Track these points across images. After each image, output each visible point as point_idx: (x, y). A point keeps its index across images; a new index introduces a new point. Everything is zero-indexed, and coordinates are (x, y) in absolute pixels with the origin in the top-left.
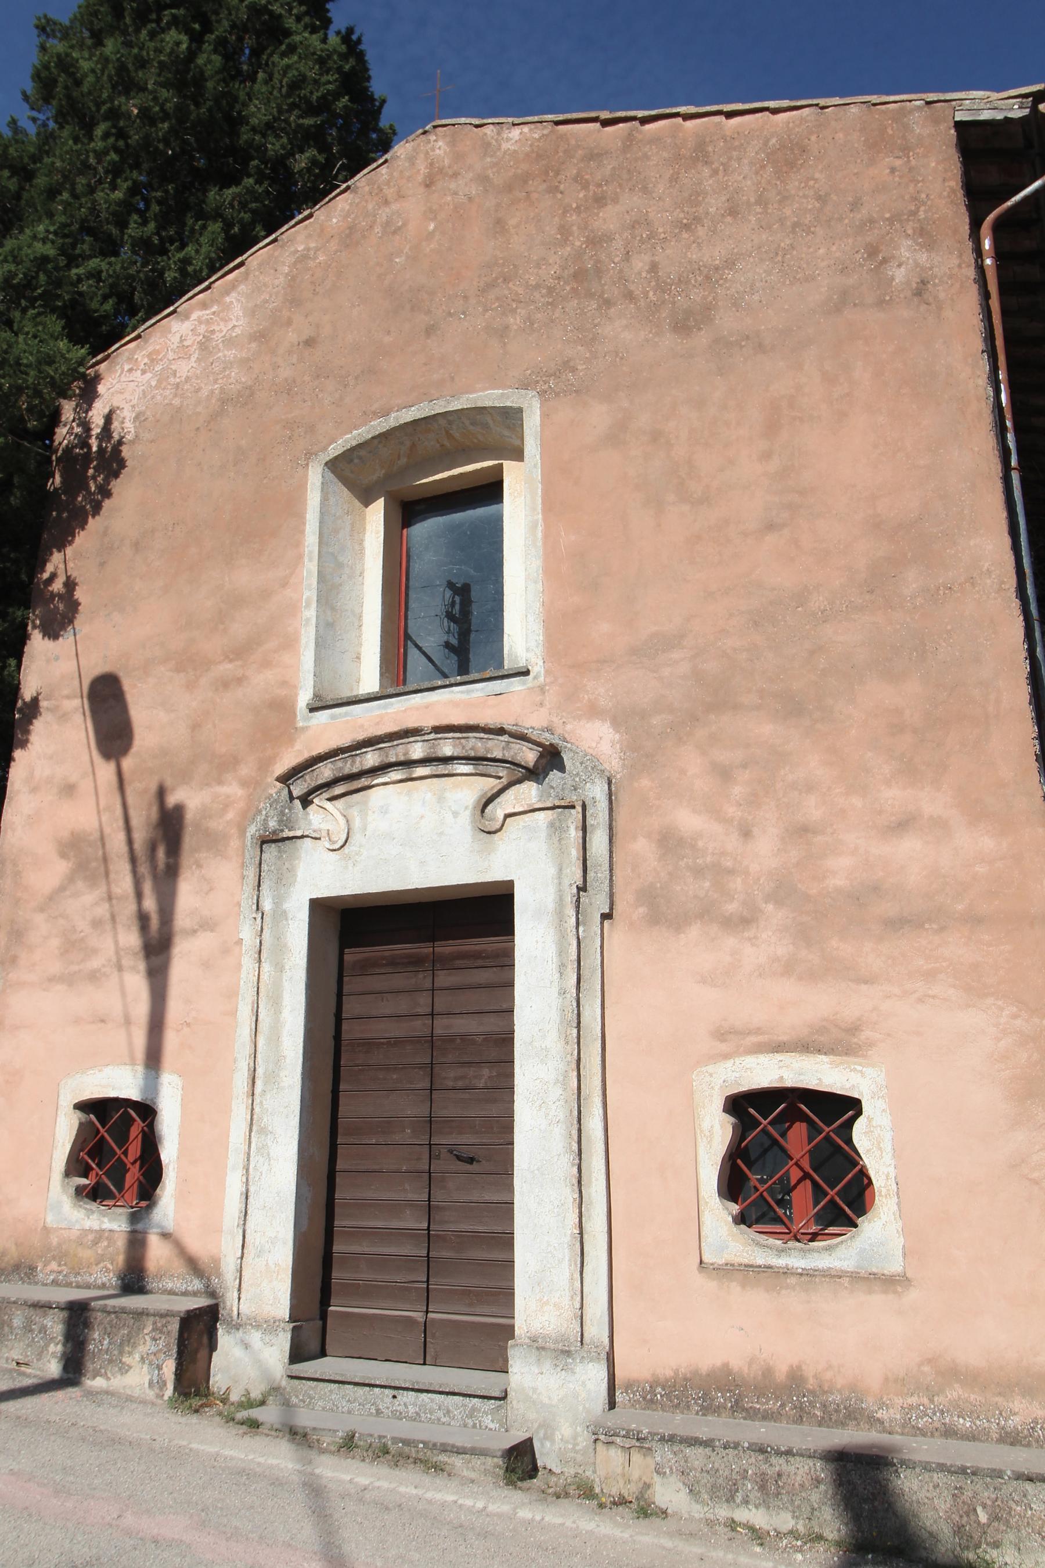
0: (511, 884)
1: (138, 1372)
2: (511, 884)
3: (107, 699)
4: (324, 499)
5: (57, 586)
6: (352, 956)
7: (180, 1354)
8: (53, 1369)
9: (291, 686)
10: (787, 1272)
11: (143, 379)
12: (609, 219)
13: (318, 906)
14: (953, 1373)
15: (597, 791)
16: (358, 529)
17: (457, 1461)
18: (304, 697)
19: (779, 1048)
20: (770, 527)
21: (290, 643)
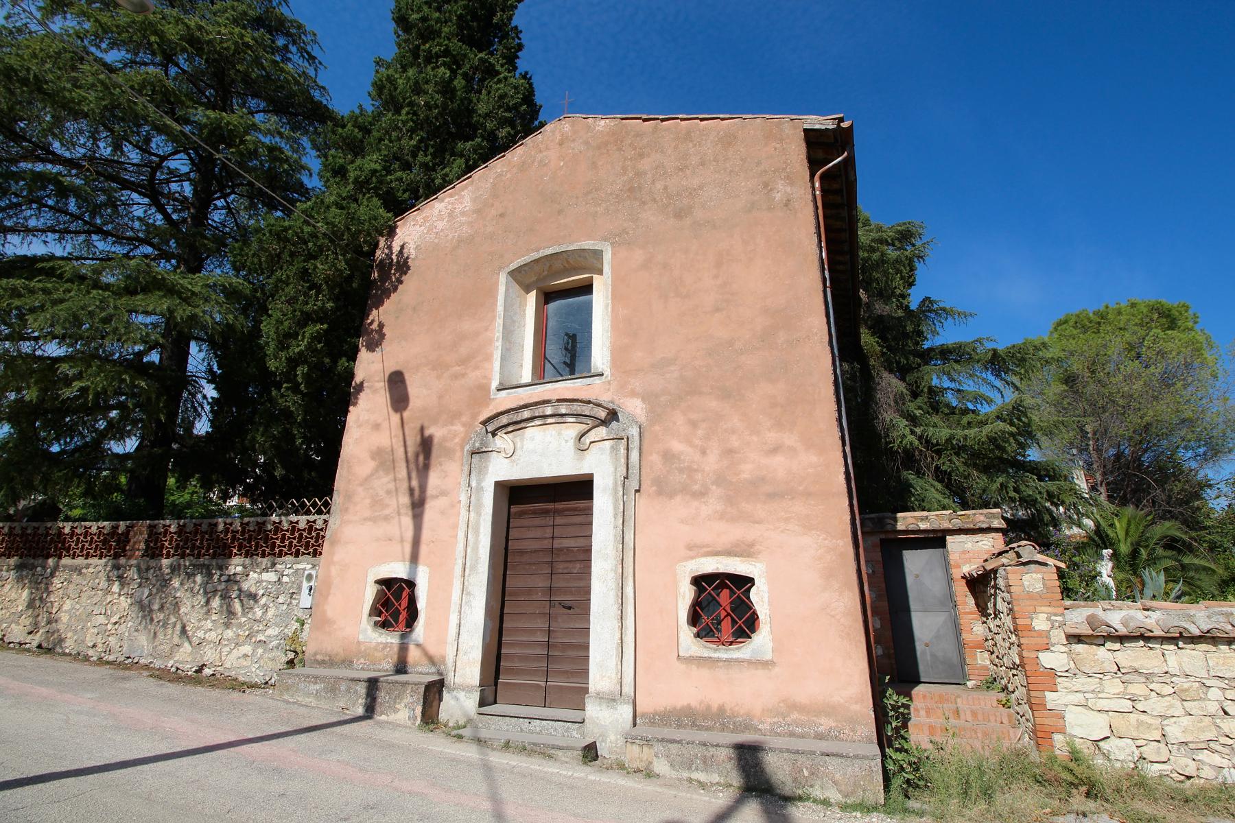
3: (397, 382)
5: (375, 326)
6: (514, 509)
7: (424, 703)
8: (360, 711)
12: (645, 164)
13: (499, 485)
14: (794, 707)
16: (523, 305)
18: (495, 384)
20: (718, 310)
21: (489, 358)
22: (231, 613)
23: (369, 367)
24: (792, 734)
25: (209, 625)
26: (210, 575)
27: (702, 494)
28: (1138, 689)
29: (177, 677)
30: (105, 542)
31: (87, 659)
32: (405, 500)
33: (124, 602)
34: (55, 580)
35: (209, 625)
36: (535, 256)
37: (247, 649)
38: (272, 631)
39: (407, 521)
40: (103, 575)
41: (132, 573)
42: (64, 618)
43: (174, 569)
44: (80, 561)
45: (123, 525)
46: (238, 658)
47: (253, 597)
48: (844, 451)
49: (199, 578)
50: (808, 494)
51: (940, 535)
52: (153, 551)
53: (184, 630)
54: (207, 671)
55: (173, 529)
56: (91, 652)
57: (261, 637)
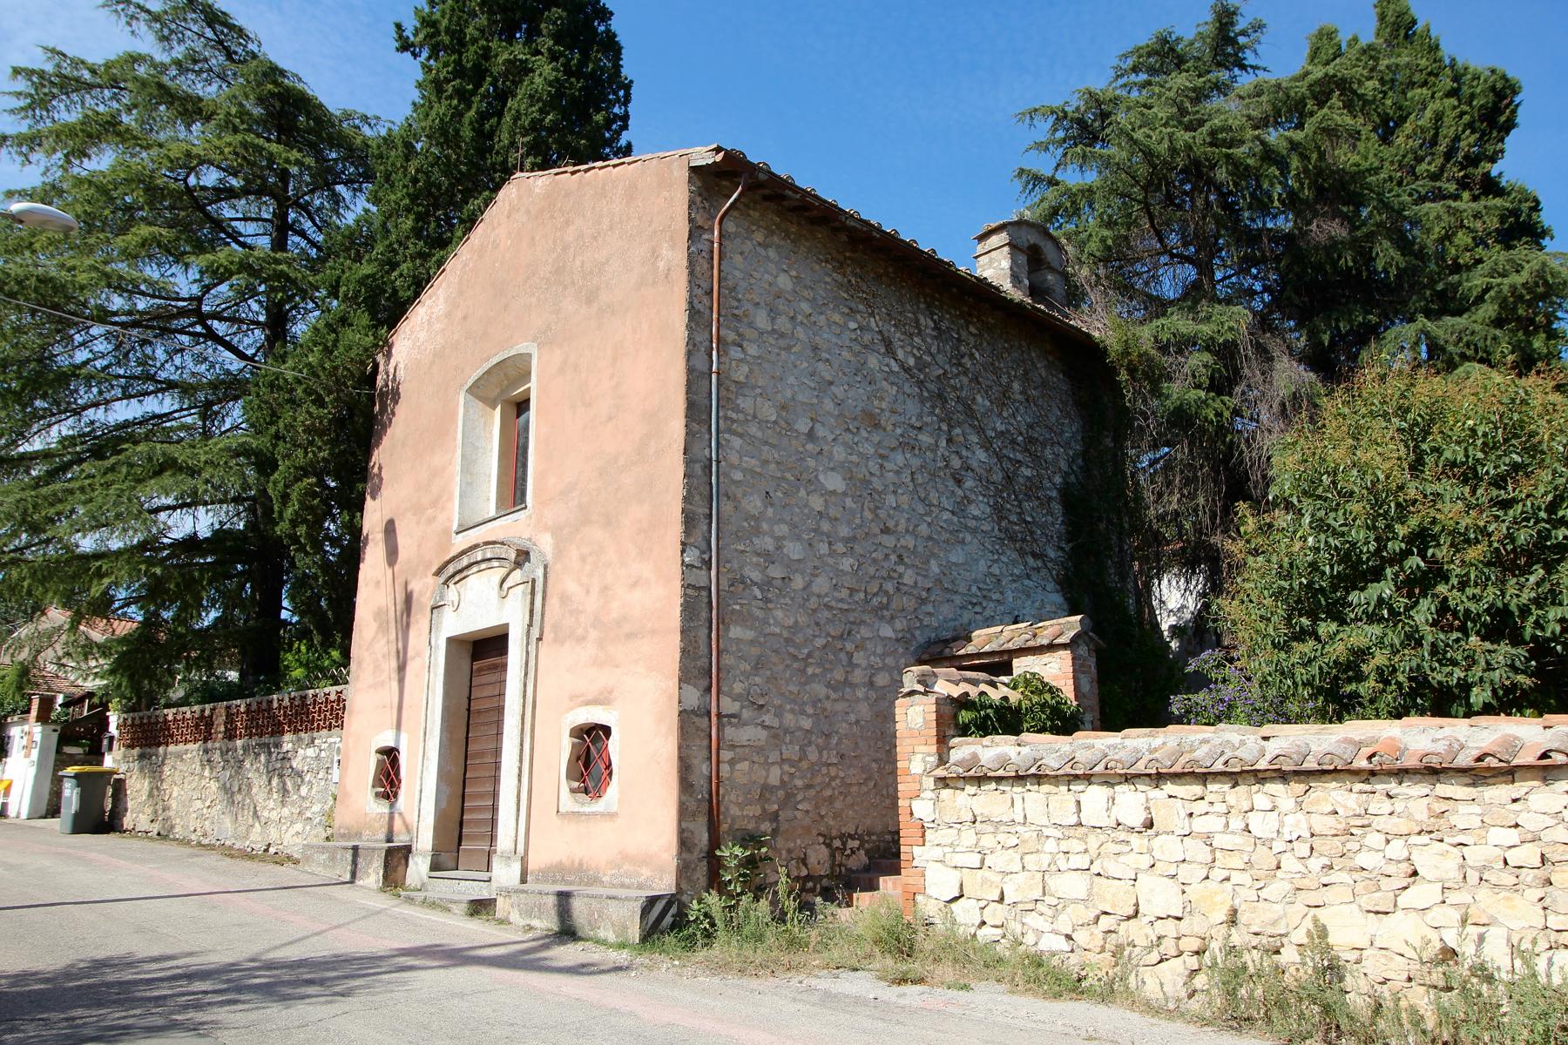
0: (506, 626)
1: (373, 875)
2: (506, 626)
3: (390, 529)
4: (466, 411)
5: (376, 470)
6: (476, 665)
7: (386, 867)
8: (348, 877)
9: (450, 520)
10: (594, 814)
11: (408, 343)
12: (570, 234)
13: (450, 641)
14: (626, 857)
15: (540, 573)
16: (488, 425)
17: (453, 906)
18: (455, 527)
19: (588, 703)
20: (610, 418)
21: (450, 498)
22: (284, 791)
23: (373, 517)
24: (623, 886)
25: (271, 804)
26: (270, 753)
27: (582, 639)
28: (987, 841)
29: (248, 855)
30: (197, 726)
31: (189, 842)
32: (394, 664)
33: (214, 785)
34: (166, 769)
35: (271, 804)
36: (487, 366)
37: (298, 827)
38: (316, 808)
39: (395, 685)
40: (197, 760)
41: (217, 757)
42: (174, 804)
43: (246, 749)
44: (181, 747)
45: (208, 707)
46: (291, 836)
47: (300, 775)
48: (532, 603)
49: (263, 758)
50: (653, 632)
51: (1006, 657)
52: (230, 735)
53: (255, 812)
54: (272, 850)
55: (242, 709)
56: (193, 837)
57: (308, 815)
